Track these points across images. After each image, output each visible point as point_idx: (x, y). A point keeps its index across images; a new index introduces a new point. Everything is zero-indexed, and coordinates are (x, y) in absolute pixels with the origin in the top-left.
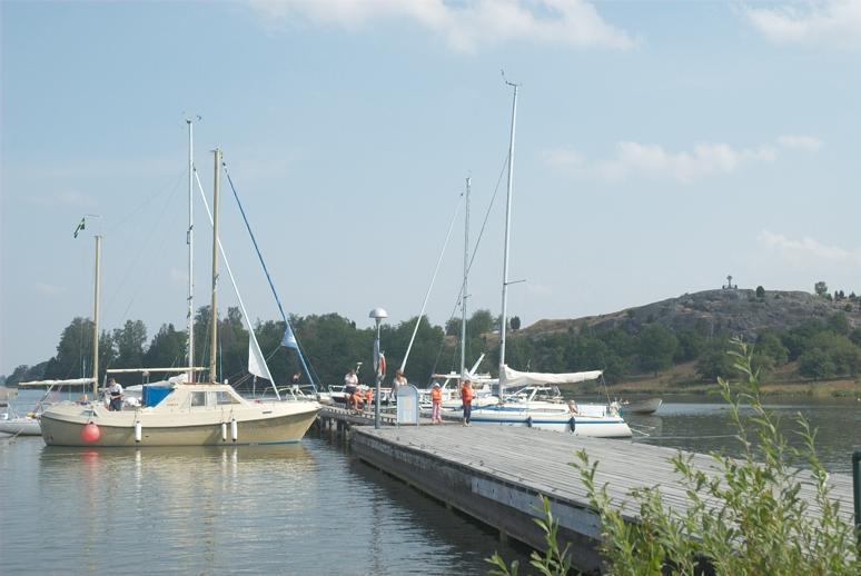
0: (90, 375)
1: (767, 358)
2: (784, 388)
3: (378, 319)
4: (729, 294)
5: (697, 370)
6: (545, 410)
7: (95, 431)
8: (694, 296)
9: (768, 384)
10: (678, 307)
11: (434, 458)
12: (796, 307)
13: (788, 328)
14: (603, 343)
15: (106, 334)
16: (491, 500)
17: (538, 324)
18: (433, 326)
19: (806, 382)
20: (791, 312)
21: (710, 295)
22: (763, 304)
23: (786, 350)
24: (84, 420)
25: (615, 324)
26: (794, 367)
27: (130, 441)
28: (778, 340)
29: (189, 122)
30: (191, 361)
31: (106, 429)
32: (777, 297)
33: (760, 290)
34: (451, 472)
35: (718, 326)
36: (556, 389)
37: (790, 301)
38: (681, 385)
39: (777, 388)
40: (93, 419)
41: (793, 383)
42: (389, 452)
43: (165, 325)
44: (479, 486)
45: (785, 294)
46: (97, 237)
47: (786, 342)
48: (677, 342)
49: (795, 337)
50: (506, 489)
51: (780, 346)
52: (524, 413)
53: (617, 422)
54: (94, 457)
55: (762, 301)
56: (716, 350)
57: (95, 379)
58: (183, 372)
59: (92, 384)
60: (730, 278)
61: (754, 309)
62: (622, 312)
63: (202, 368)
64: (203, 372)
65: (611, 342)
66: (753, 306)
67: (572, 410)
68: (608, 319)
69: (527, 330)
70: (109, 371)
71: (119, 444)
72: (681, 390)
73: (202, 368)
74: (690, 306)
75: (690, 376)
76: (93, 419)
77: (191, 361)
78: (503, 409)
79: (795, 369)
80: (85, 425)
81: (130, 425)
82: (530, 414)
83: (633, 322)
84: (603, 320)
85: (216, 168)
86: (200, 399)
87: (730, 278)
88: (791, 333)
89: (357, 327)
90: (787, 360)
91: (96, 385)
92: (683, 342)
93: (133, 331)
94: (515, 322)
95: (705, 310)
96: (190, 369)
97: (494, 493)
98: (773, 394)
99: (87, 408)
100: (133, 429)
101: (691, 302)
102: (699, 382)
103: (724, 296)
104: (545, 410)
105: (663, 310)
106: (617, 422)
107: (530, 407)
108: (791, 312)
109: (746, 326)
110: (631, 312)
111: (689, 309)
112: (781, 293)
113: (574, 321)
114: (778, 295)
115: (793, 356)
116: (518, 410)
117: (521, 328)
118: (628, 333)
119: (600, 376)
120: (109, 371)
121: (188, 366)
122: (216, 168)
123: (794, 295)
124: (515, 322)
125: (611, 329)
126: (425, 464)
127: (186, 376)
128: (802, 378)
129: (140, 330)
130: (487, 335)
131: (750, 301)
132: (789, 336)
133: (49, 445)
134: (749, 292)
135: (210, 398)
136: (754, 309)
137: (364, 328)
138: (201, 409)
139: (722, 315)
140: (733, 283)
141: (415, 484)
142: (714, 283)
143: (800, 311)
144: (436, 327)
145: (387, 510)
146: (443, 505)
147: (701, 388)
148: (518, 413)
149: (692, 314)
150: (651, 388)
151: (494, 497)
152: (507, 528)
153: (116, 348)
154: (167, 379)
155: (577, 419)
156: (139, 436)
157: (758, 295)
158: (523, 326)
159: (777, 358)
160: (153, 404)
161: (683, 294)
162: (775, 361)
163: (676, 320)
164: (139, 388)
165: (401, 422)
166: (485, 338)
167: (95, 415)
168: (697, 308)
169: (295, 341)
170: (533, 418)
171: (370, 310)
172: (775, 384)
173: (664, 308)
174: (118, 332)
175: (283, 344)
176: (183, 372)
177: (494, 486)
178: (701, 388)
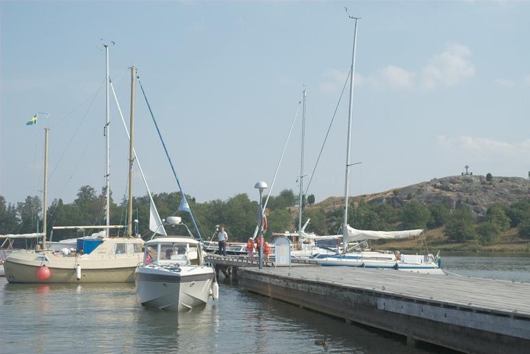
0: (41, 231)
1: (495, 225)
2: (508, 247)
3: (261, 190)
4: (467, 179)
5: (445, 233)
6: (377, 258)
7: (47, 272)
8: (441, 181)
9: (496, 244)
10: (430, 188)
11: (332, 286)
12: (516, 189)
13: (510, 203)
14: (376, 214)
15: (12, 206)
16: (398, 314)
17: (328, 199)
18: (251, 201)
19: (524, 243)
20: (511, 192)
21: (453, 180)
22: (492, 186)
23: (509, 219)
24: (38, 263)
25: (384, 200)
26: (515, 231)
27: (72, 279)
28: (503, 212)
29: (106, 46)
30: (108, 222)
31: (54, 270)
32: (501, 181)
33: (489, 176)
34: (353, 296)
35: (459, 202)
36: (365, 243)
37: (511, 184)
38: (433, 244)
39: (503, 247)
40: (45, 263)
41: (514, 243)
42: (283, 284)
43: (55, 199)
44: (382, 304)
45: (507, 179)
46: (46, 129)
47: (509, 214)
48: (430, 213)
49: (515, 210)
50: (416, 305)
51: (504, 217)
52: (360, 261)
53: (433, 268)
54: (47, 289)
55: (490, 184)
56: (458, 219)
57: (44, 234)
58: (102, 230)
59: (43, 237)
60: (467, 167)
61: (485, 190)
62: (389, 192)
63: (122, 226)
64: (121, 229)
65: (381, 213)
66: (484, 187)
67: (398, 258)
68: (379, 196)
69: (320, 204)
70: (54, 228)
71: (65, 280)
72: (433, 247)
73: (122, 226)
74: (438, 188)
75: (439, 238)
76: (45, 263)
77: (108, 222)
78: (344, 257)
79: (516, 233)
80: (40, 267)
81: (73, 268)
82: (364, 261)
83: (397, 199)
84: (375, 197)
85: (132, 80)
86: (121, 249)
87: (467, 167)
88: (512, 207)
89: (196, 201)
90: (509, 227)
91: (45, 238)
92: (434, 214)
93: (31, 205)
94: (312, 199)
95: (448, 189)
96: (108, 226)
97: (392, 306)
98: (500, 251)
99: (40, 255)
100: (75, 270)
101: (439, 184)
102: (446, 242)
103: (463, 180)
104: (377, 258)
105: (419, 190)
106: (433, 268)
107: (364, 256)
108: (511, 192)
109: (479, 202)
110: (395, 192)
111: (438, 190)
112: (504, 178)
113: (354, 198)
114: (502, 180)
115: (514, 225)
116: (360, 258)
117: (316, 202)
118: (394, 206)
119: (422, 233)
120: (54, 228)
121: (105, 225)
122: (132, 80)
123: (514, 179)
124: (312, 199)
125: (381, 204)
126: (322, 291)
127: (104, 232)
128: (521, 240)
129: (37, 204)
130: (292, 209)
131: (482, 184)
132: (510, 209)
133: (10, 282)
134: (481, 177)
135: (130, 248)
136: (485, 190)
137: (202, 202)
138: (123, 256)
139: (461, 193)
140: (469, 171)
141: (307, 306)
142: (456, 171)
143: (518, 192)
144: (254, 202)
145: (270, 324)
146: (343, 320)
147: (448, 246)
148: (355, 260)
149: (440, 193)
150: (412, 247)
151: (403, 311)
152: (415, 334)
153: (19, 216)
154: (90, 235)
155: (399, 265)
156: (79, 276)
157: (488, 180)
158: (316, 202)
159: (503, 225)
160: (88, 252)
161: (433, 178)
162: (501, 228)
163: (429, 197)
164: (74, 241)
165: (279, 264)
166: (289, 210)
167: (46, 260)
168: (443, 189)
169: (188, 207)
170: (366, 264)
171: (255, 184)
172: (502, 244)
173: (420, 189)
174: (20, 205)
175: (179, 209)
176: (102, 230)
177: (403, 303)
178: (448, 246)
